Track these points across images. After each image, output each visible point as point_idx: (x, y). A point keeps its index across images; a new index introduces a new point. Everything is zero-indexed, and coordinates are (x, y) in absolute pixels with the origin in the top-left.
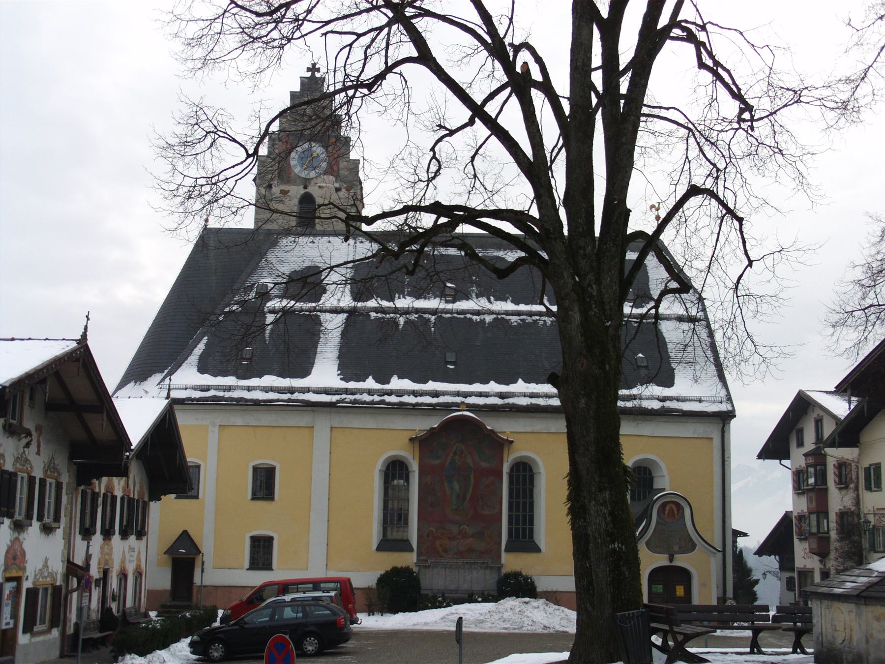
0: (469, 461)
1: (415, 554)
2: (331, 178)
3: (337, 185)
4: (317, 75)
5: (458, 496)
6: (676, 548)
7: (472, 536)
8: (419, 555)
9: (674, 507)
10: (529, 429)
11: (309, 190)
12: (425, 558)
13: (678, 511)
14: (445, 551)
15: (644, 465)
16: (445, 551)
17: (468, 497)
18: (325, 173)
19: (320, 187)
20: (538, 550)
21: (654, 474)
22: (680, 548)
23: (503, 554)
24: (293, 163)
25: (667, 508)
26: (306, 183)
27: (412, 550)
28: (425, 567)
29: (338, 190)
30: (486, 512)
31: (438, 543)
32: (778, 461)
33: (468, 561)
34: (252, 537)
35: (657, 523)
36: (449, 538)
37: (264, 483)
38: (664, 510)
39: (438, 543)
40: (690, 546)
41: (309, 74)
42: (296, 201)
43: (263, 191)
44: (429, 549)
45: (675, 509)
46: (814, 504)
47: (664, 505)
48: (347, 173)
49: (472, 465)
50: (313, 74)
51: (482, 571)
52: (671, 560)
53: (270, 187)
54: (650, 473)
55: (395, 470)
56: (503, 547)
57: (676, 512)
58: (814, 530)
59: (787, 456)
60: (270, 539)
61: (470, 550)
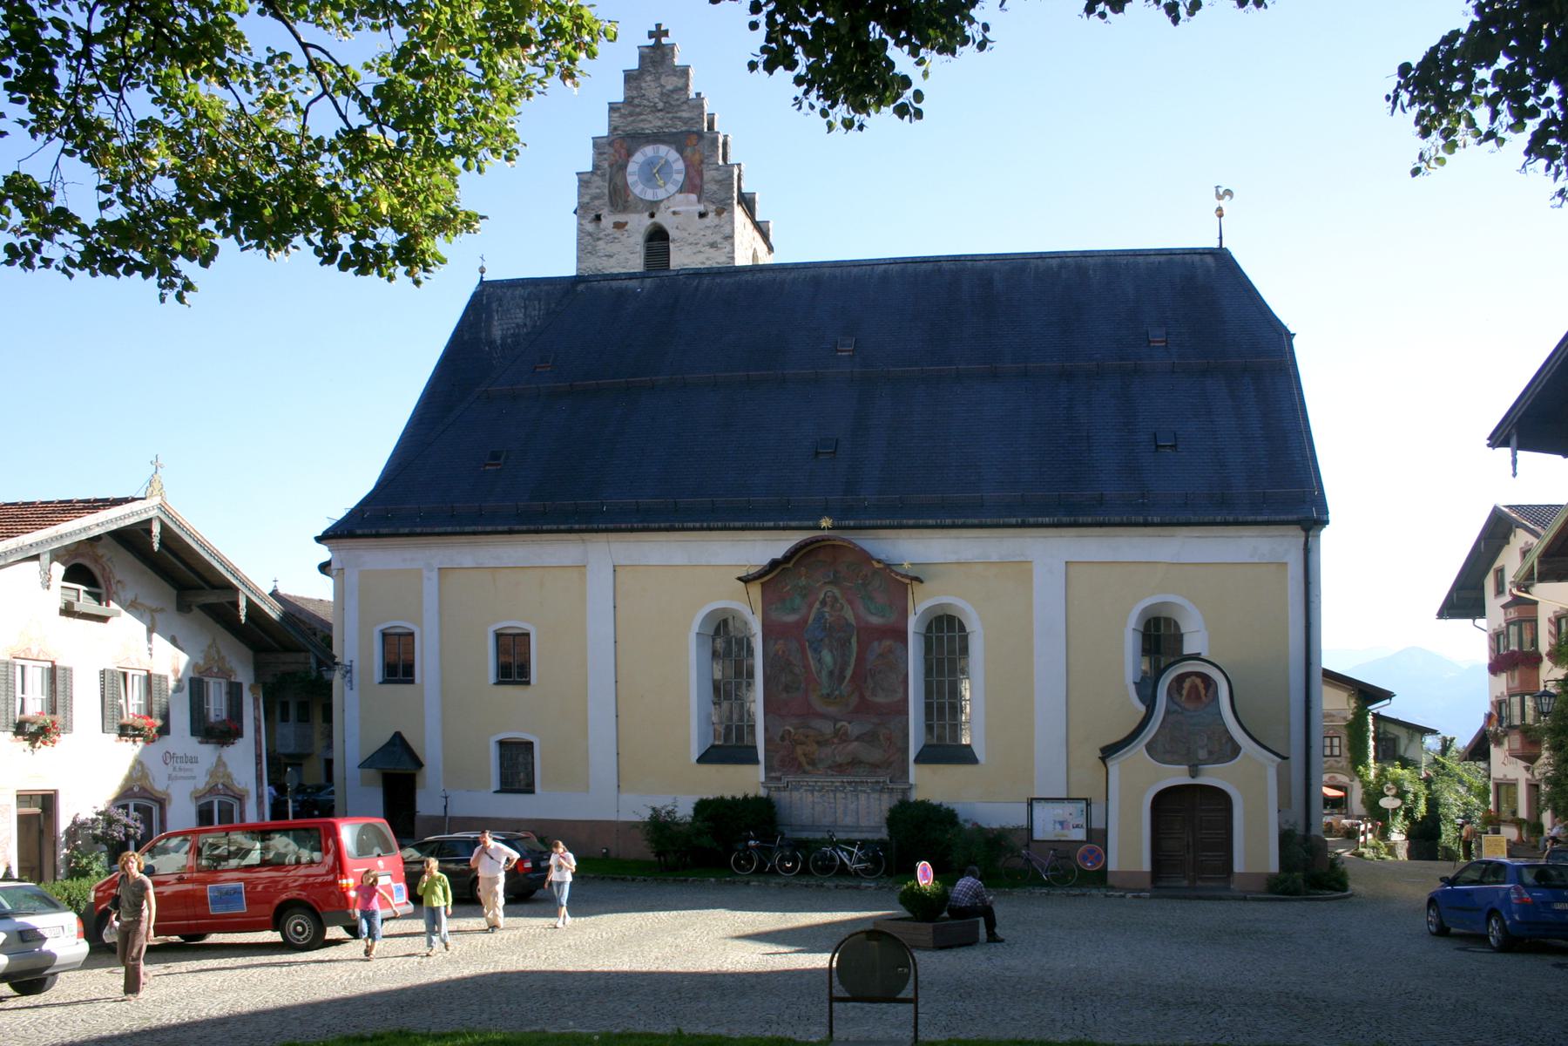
0: (849, 615)
1: (762, 767)
2: (693, 197)
3: (701, 208)
5: (831, 673)
6: (1202, 754)
7: (857, 738)
8: (768, 769)
9: (1198, 681)
11: (658, 219)
12: (778, 774)
13: (1207, 688)
14: (813, 763)
15: (1164, 614)
16: (813, 763)
17: (849, 673)
19: (674, 213)
22: (1210, 753)
23: (912, 768)
24: (630, 179)
25: (1187, 685)
26: (652, 208)
27: (756, 762)
29: (702, 215)
30: (881, 699)
31: (799, 750)
32: (1470, 621)
33: (851, 779)
35: (1168, 712)
36: (818, 743)
39: (799, 750)
41: (652, 42)
44: (785, 760)
46: (1517, 682)
47: (1181, 679)
48: (715, 187)
49: (852, 620)
50: (658, 41)
51: (876, 795)
53: (598, 218)
57: (1203, 692)
58: (1517, 722)
59: (1482, 615)
61: (855, 762)
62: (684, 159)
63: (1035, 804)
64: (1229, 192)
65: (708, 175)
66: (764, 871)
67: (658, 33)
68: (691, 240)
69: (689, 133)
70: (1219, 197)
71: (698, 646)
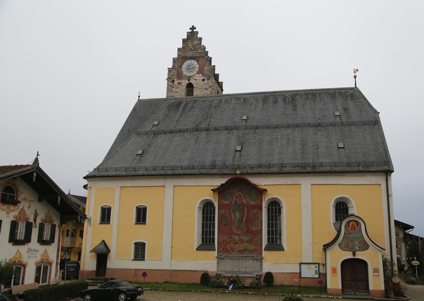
0: (245, 201)
1: (216, 252)
2: (201, 75)
3: (203, 78)
4: (195, 30)
5: (239, 220)
6: (357, 248)
7: (246, 242)
8: (218, 252)
10: (276, 183)
11: (191, 81)
12: (221, 254)
14: (232, 250)
16: (232, 250)
17: (244, 220)
18: (197, 73)
19: (195, 80)
20: (283, 249)
21: (348, 206)
23: (263, 252)
24: (183, 70)
25: (351, 224)
26: (189, 78)
28: (221, 259)
29: (203, 80)
30: (254, 229)
31: (228, 245)
34: (136, 244)
37: (141, 215)
38: (349, 226)
39: (228, 245)
40: (365, 247)
42: (184, 87)
43: (170, 84)
45: (356, 225)
47: (349, 222)
48: (207, 72)
49: (246, 203)
52: (354, 255)
53: (173, 81)
54: (346, 205)
55: (207, 208)
56: (263, 248)
57: (356, 227)
60: (144, 244)
61: (245, 250)
62: (198, 64)
64: (357, 70)
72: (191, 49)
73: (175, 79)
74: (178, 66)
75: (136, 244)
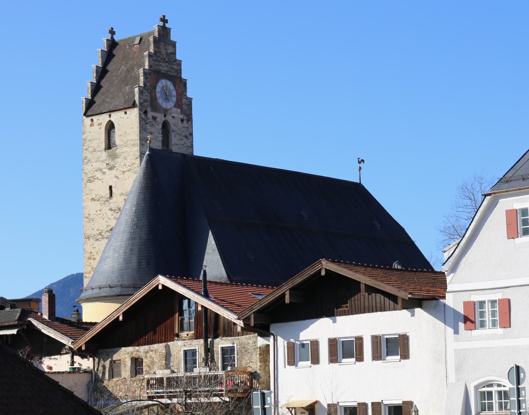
29: (182, 120)
34: (507, 212)
43: (143, 116)
62: (176, 90)
63: (58, 315)
64: (363, 161)
65: (184, 101)
66: (350, 408)
67: (164, 20)
68: (179, 132)
69: (176, 76)
70: (359, 163)
71: (180, 284)
72: (164, 59)
73: (149, 109)
74: (150, 86)
75: (507, 212)
